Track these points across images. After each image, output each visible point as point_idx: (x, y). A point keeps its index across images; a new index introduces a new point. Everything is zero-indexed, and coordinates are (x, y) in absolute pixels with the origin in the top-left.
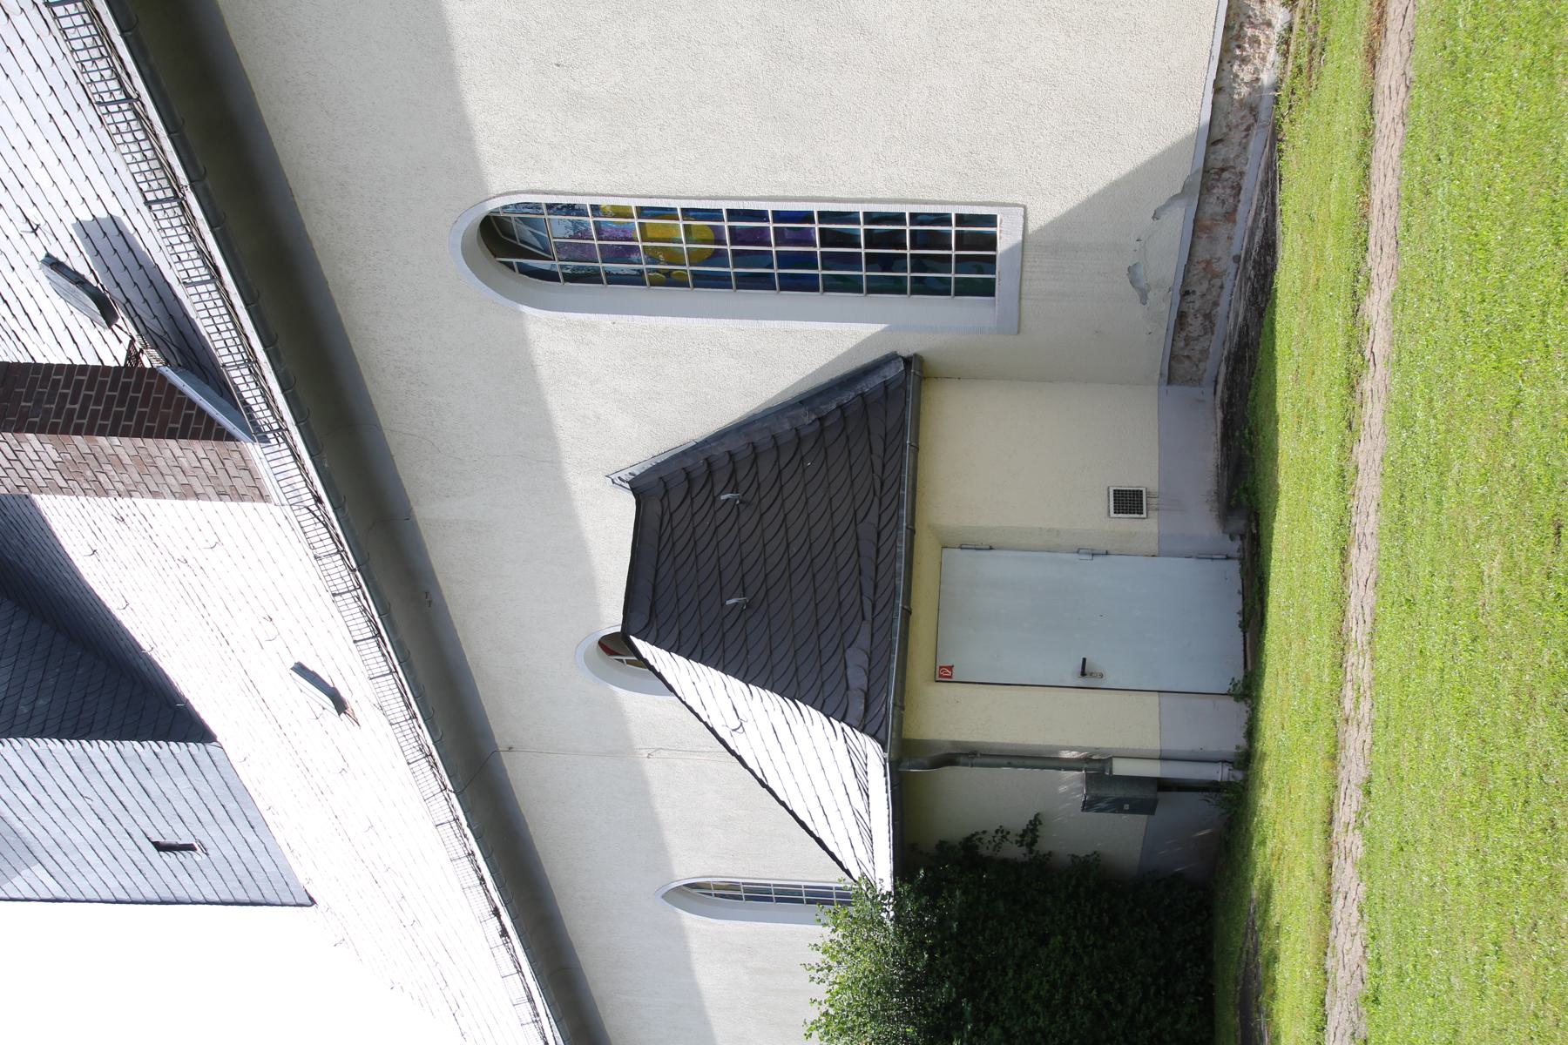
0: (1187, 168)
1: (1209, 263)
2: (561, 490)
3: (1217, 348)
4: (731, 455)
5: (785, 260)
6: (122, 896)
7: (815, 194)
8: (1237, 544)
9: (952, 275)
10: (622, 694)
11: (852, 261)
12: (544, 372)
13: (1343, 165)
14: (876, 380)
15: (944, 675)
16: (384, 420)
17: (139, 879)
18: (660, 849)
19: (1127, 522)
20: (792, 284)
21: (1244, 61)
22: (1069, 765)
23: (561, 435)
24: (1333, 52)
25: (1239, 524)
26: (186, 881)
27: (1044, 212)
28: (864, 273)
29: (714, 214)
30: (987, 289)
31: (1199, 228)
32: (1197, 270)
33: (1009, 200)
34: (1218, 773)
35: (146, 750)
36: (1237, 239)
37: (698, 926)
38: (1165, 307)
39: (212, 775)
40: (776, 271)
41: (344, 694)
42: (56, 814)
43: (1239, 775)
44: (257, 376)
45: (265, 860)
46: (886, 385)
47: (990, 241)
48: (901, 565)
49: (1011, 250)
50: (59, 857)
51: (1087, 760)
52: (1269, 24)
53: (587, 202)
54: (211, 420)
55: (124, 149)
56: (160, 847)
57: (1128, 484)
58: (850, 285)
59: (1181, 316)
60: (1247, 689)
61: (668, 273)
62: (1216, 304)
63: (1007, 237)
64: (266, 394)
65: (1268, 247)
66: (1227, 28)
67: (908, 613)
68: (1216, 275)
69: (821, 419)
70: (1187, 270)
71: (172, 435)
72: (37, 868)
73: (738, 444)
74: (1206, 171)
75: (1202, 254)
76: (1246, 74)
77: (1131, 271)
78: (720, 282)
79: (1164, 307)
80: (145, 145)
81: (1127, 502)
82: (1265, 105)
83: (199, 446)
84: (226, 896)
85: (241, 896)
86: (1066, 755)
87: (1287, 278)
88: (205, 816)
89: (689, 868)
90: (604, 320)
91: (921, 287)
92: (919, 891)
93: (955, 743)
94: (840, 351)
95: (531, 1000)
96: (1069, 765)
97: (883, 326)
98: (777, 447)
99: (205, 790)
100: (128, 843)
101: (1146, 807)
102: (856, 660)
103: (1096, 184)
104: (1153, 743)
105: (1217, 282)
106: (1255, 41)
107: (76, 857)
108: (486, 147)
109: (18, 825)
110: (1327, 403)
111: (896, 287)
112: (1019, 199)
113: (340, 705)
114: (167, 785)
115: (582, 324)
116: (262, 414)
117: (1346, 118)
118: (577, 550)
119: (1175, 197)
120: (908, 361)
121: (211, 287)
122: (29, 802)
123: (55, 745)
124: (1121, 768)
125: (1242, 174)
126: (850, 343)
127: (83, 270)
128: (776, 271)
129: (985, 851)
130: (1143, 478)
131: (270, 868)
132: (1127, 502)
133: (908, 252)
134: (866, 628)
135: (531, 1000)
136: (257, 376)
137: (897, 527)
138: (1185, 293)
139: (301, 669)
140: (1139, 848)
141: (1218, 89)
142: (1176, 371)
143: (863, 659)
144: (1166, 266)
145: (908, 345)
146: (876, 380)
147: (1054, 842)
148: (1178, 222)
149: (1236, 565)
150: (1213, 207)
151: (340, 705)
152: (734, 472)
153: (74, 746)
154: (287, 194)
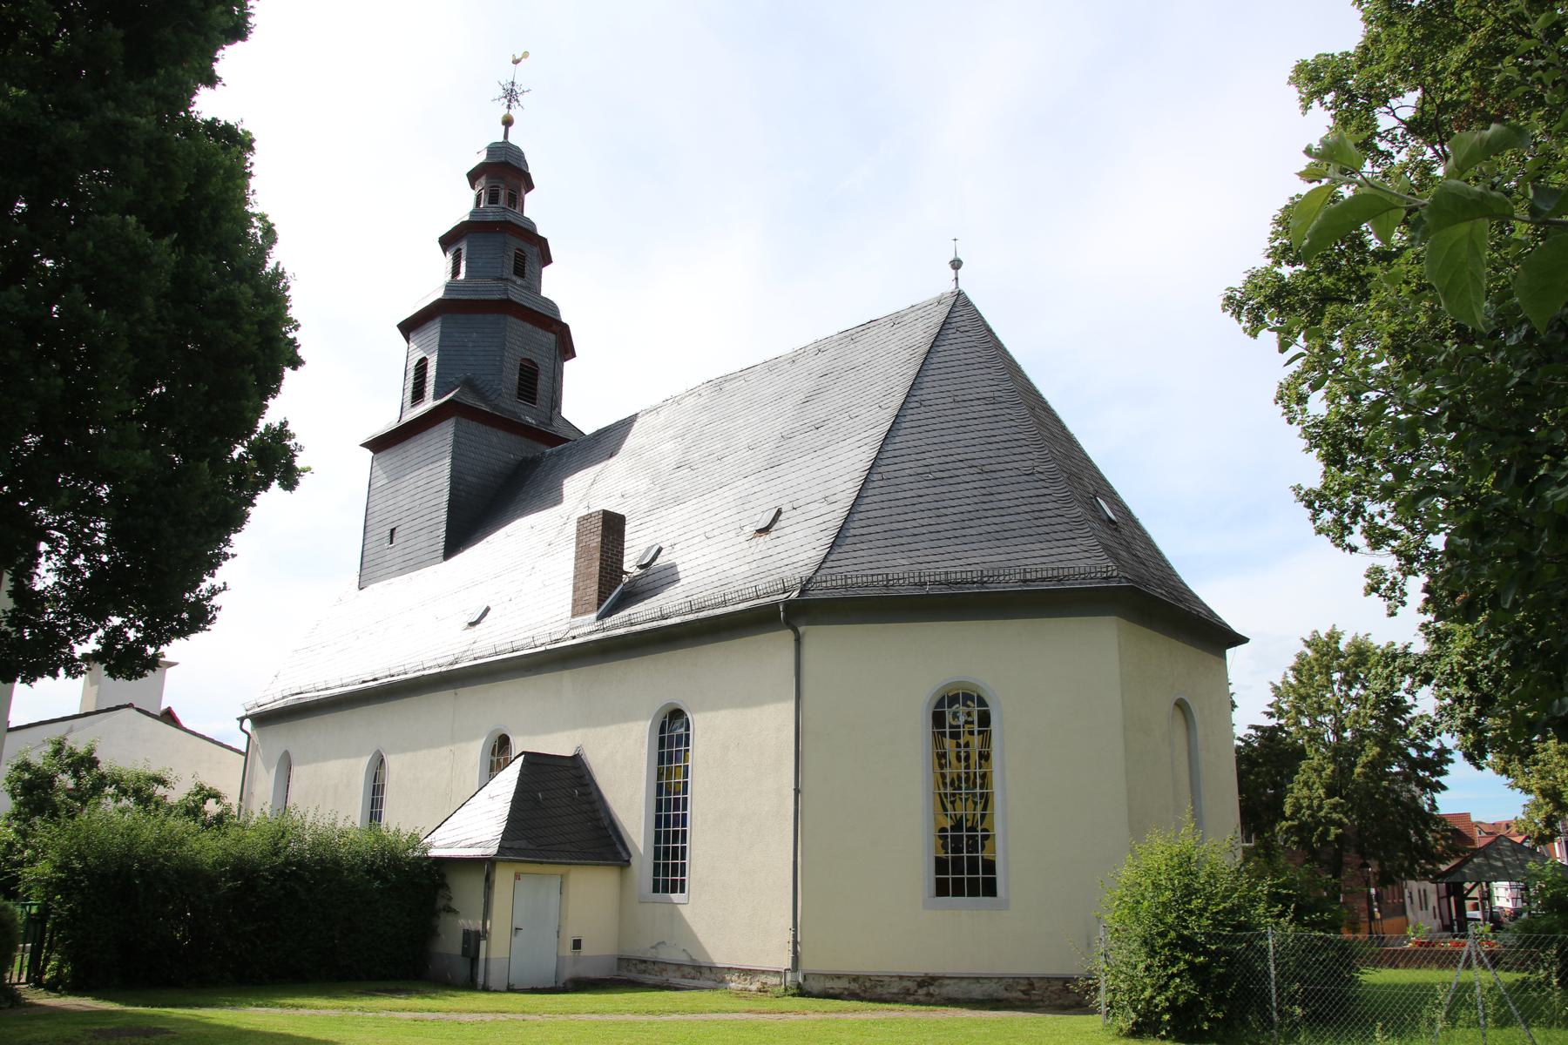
0: (702, 961)
2: (575, 727)
3: (633, 975)
4: (590, 794)
5: (667, 817)
6: (369, 512)
8: (561, 986)
11: (667, 841)
12: (624, 726)
13: (715, 1007)
14: (621, 849)
15: (517, 877)
17: (377, 519)
18: (403, 750)
19: (570, 944)
20: (658, 819)
21: (739, 977)
22: (484, 924)
23: (598, 729)
24: (747, 1002)
26: (374, 539)
27: (686, 911)
29: (685, 792)
30: (656, 890)
31: (679, 966)
32: (663, 966)
34: (480, 980)
35: (442, 531)
36: (676, 980)
37: (362, 764)
39: (426, 557)
40: (663, 813)
41: (478, 627)
42: (412, 493)
44: (622, 625)
45: (383, 572)
46: (619, 853)
47: (674, 891)
48: (558, 860)
50: (391, 490)
51: (486, 931)
53: (690, 748)
54: (604, 601)
56: (393, 531)
57: (583, 944)
58: (657, 840)
59: (645, 962)
60: (510, 989)
61: (663, 774)
63: (676, 897)
64: (615, 627)
65: (677, 989)
66: (750, 970)
67: (541, 863)
68: (661, 973)
69: (606, 828)
70: (662, 963)
71: (599, 588)
72: (386, 481)
73: (595, 795)
74: (700, 967)
75: (669, 967)
76: (734, 978)
77: (663, 943)
78: (659, 792)
79: (649, 955)
81: (577, 944)
82: (725, 986)
83: (595, 596)
84: (366, 553)
85: (365, 560)
86: (488, 923)
88: (407, 551)
89: (392, 762)
90: (645, 750)
91: (656, 866)
92: (429, 867)
93: (493, 882)
94: (632, 837)
95: (327, 689)
96: (484, 924)
98: (594, 811)
99: (420, 553)
100: (395, 518)
101: (465, 952)
102: (523, 844)
103: (695, 929)
104: (493, 955)
106: (746, 980)
107: (390, 497)
108: (709, 715)
109: (408, 477)
110: (636, 1006)
111: (657, 856)
113: (472, 624)
114: (423, 538)
115: (643, 742)
116: (609, 621)
117: (728, 1006)
118: (548, 730)
120: (628, 861)
122: (419, 483)
123: (446, 498)
124: (483, 944)
126: (635, 840)
127: (658, 561)
128: (663, 813)
129: (441, 892)
130: (586, 950)
131: (379, 573)
132: (577, 944)
133: (981, 876)
134: (534, 847)
135: (327, 689)
136: (622, 625)
137: (571, 859)
138: (654, 963)
139: (488, 609)
141: (729, 969)
142: (623, 961)
143: (524, 846)
144: (665, 955)
145: (634, 861)
146: (621, 849)
147: (445, 921)
148: (681, 958)
149: (554, 985)
150: (687, 970)
151: (472, 624)
152: (585, 795)
153: (445, 505)
154: (692, 645)
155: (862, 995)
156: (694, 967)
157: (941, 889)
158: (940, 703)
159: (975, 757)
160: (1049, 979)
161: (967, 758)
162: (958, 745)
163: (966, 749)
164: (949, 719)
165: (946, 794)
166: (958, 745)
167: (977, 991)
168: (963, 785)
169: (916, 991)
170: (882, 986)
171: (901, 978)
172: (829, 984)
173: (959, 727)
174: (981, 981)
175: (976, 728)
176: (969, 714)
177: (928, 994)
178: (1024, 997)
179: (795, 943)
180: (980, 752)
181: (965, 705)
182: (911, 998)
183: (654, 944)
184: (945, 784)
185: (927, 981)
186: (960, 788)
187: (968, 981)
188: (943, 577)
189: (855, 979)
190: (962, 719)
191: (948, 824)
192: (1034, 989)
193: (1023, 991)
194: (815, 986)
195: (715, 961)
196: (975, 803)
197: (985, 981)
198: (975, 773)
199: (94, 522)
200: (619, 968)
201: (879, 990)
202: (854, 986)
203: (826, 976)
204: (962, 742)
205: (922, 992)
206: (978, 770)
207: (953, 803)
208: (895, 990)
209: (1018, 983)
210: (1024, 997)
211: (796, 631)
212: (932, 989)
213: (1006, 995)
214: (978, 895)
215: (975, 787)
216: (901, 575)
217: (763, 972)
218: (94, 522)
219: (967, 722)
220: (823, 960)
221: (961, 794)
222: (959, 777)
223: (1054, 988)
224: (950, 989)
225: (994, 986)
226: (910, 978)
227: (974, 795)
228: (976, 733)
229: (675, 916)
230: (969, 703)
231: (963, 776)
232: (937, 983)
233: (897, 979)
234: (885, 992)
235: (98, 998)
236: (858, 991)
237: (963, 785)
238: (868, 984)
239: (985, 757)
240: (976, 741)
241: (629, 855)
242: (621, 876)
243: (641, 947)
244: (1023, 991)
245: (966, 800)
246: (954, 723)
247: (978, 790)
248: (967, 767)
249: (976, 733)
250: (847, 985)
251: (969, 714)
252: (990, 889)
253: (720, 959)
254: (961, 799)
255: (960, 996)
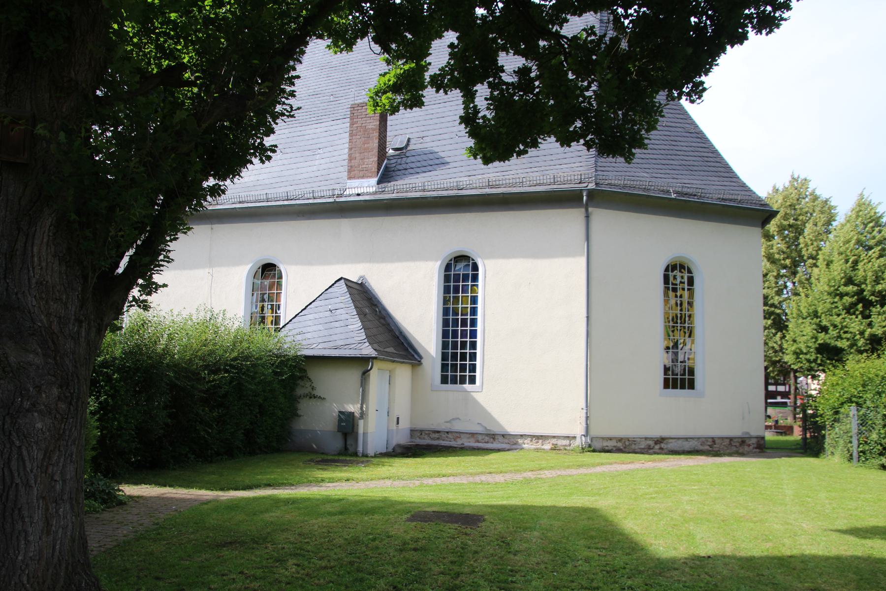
0: (496, 430)
1: (460, 437)
7: (486, 341)
9: (449, 374)
10: (250, 265)
16: (485, 213)
21: (531, 441)
25: (399, 450)
28: (450, 351)
30: (444, 380)
33: (484, 387)
34: (360, 449)
38: (443, 427)
43: (361, 455)
49: (465, 389)
52: (543, 445)
54: (381, 168)
55: (541, 177)
59: (438, 432)
62: (443, 440)
66: (542, 436)
70: (457, 432)
75: (462, 436)
79: (443, 427)
80: (417, 188)
86: (364, 406)
87: (451, 460)
91: (443, 365)
97: (435, 356)
103: (489, 409)
105: (453, 440)
106: (537, 442)
111: (443, 359)
112: (484, 390)
119: (486, 428)
121: (265, 198)
125: (492, 443)
140: (302, 427)
144: (458, 427)
148: (478, 429)
155: (624, 450)
156: (487, 435)
157: (666, 385)
158: (667, 269)
159: (685, 305)
160: (722, 438)
161: (681, 305)
162: (676, 296)
163: (681, 299)
164: (671, 279)
165: (669, 326)
166: (676, 296)
167: (687, 446)
168: (679, 321)
169: (654, 447)
170: (635, 444)
171: (646, 439)
172: (605, 444)
173: (676, 285)
174: (689, 440)
175: (686, 287)
176: (682, 277)
177: (661, 448)
178: (711, 449)
179: (587, 418)
180: (688, 301)
181: (680, 271)
182: (651, 451)
183: (448, 420)
184: (669, 322)
185: (660, 440)
186: (677, 323)
187: (682, 440)
188: (455, 184)
189: (620, 440)
190: (678, 281)
191: (671, 344)
192: (715, 444)
193: (709, 445)
194: (598, 445)
195: (509, 430)
196: (685, 333)
197: (691, 440)
198: (685, 314)
199: (407, 7)
200: (412, 436)
201: (633, 446)
202: (620, 445)
203: (603, 439)
204: (678, 294)
205: (657, 447)
206: (687, 312)
207: (673, 331)
208: (643, 447)
209: (707, 441)
210: (711, 449)
211: (587, 210)
212: (663, 445)
213: (701, 448)
214: (677, 388)
215: (685, 322)
216: (474, 182)
217: (554, 437)
218: (408, 7)
219: (681, 282)
220: (601, 430)
221: (677, 326)
222: (677, 316)
223: (725, 444)
224: (673, 445)
225: (696, 443)
226: (651, 439)
227: (684, 327)
228: (686, 289)
229: (468, 398)
230: (683, 270)
231: (679, 315)
232: (665, 442)
233: (644, 440)
234: (636, 448)
235: (207, 489)
236: (622, 448)
237: (679, 321)
238: (627, 443)
239: (690, 304)
240: (686, 294)
241: (421, 357)
242: (412, 372)
243: (437, 421)
244: (709, 445)
245: (680, 330)
246: (674, 282)
247: (686, 325)
248: (681, 310)
249: (686, 289)
250: (615, 444)
251: (682, 277)
252: (692, 386)
253: (512, 427)
254: (677, 330)
255: (678, 449)
